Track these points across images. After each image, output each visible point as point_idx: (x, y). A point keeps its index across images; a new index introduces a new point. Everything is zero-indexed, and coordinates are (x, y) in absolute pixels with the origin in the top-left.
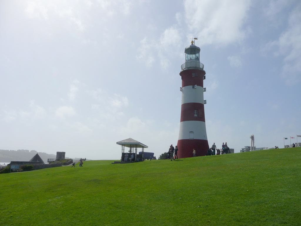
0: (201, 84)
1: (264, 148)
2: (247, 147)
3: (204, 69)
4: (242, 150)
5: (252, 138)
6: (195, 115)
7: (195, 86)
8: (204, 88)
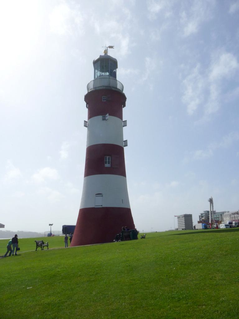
0: (119, 115)
1: (225, 212)
2: (207, 212)
3: (124, 92)
4: (200, 215)
5: (211, 201)
6: (105, 165)
7: (106, 116)
8: (123, 120)
